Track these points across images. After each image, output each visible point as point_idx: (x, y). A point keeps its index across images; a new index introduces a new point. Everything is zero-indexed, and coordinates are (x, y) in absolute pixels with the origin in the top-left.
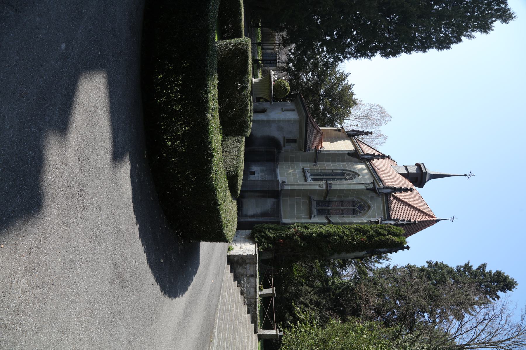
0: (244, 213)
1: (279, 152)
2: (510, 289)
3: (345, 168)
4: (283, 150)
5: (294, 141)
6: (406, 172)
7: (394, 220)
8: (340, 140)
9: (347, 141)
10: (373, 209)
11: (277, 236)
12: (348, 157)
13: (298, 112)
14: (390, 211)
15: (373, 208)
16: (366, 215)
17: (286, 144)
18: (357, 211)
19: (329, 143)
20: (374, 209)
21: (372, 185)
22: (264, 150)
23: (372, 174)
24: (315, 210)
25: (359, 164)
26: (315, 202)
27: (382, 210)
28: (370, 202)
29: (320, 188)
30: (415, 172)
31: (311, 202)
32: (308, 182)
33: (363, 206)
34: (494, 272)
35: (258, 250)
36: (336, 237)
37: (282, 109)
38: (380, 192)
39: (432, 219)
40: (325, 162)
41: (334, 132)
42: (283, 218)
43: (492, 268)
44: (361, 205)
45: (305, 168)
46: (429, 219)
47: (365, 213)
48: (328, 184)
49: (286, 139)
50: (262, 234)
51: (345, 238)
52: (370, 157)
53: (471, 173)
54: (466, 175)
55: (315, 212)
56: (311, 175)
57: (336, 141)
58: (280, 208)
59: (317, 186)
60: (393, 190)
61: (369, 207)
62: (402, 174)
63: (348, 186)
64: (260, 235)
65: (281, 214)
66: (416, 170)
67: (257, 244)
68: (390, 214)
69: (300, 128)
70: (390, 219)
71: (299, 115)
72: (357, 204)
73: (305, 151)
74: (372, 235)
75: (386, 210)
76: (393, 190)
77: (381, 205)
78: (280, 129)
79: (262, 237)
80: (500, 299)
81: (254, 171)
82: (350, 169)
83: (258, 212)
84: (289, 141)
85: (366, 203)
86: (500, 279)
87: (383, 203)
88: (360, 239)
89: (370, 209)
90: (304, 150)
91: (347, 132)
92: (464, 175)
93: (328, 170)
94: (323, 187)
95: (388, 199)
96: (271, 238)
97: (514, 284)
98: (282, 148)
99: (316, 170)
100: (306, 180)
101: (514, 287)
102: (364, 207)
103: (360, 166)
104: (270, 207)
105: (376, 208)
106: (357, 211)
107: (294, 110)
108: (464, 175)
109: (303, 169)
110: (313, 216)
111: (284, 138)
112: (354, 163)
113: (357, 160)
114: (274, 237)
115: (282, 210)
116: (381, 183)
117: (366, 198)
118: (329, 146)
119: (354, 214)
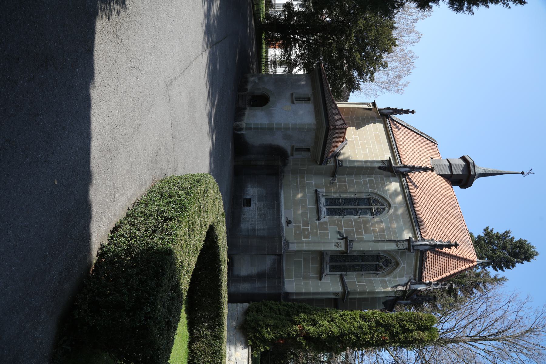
0: (236, 273)
1: (285, 165)
2: (528, 260)
3: (373, 190)
4: (291, 158)
5: (308, 150)
6: (449, 173)
7: (426, 284)
10: (402, 266)
12: (379, 170)
13: (316, 106)
15: (402, 265)
16: (392, 274)
17: (295, 153)
18: (381, 268)
21: (407, 243)
22: (263, 164)
23: (407, 204)
24: (328, 266)
27: (413, 268)
28: (399, 259)
29: (338, 249)
30: (461, 173)
31: (324, 257)
33: (390, 261)
34: (516, 240)
36: (351, 335)
38: (415, 249)
39: (471, 265)
40: (346, 176)
41: (362, 111)
43: (517, 236)
45: (319, 190)
46: (467, 266)
47: (392, 272)
48: (348, 241)
50: (257, 335)
51: (363, 336)
52: (408, 169)
53: (531, 171)
54: (523, 173)
55: (324, 212)
56: (327, 199)
59: (334, 244)
60: (432, 248)
61: (397, 264)
63: (375, 243)
64: (254, 336)
66: (462, 171)
68: (422, 275)
69: (317, 137)
70: (420, 282)
71: (317, 114)
72: (382, 258)
73: (321, 164)
74: (397, 332)
76: (432, 248)
77: (414, 262)
78: (287, 137)
80: (514, 268)
81: (249, 197)
83: (253, 272)
84: (298, 149)
85: (394, 258)
86: (522, 251)
87: (417, 260)
88: (381, 337)
89: (398, 267)
90: (319, 163)
91: (380, 110)
92: (521, 173)
93: (349, 192)
94: (341, 247)
95: (423, 256)
96: (268, 340)
97: (533, 254)
98: (289, 157)
100: (319, 219)
102: (390, 263)
103: (394, 186)
104: (269, 266)
105: (405, 265)
106: (381, 268)
108: (521, 173)
109: (316, 190)
111: (293, 147)
113: (390, 173)
115: (285, 268)
116: (417, 228)
119: (376, 271)
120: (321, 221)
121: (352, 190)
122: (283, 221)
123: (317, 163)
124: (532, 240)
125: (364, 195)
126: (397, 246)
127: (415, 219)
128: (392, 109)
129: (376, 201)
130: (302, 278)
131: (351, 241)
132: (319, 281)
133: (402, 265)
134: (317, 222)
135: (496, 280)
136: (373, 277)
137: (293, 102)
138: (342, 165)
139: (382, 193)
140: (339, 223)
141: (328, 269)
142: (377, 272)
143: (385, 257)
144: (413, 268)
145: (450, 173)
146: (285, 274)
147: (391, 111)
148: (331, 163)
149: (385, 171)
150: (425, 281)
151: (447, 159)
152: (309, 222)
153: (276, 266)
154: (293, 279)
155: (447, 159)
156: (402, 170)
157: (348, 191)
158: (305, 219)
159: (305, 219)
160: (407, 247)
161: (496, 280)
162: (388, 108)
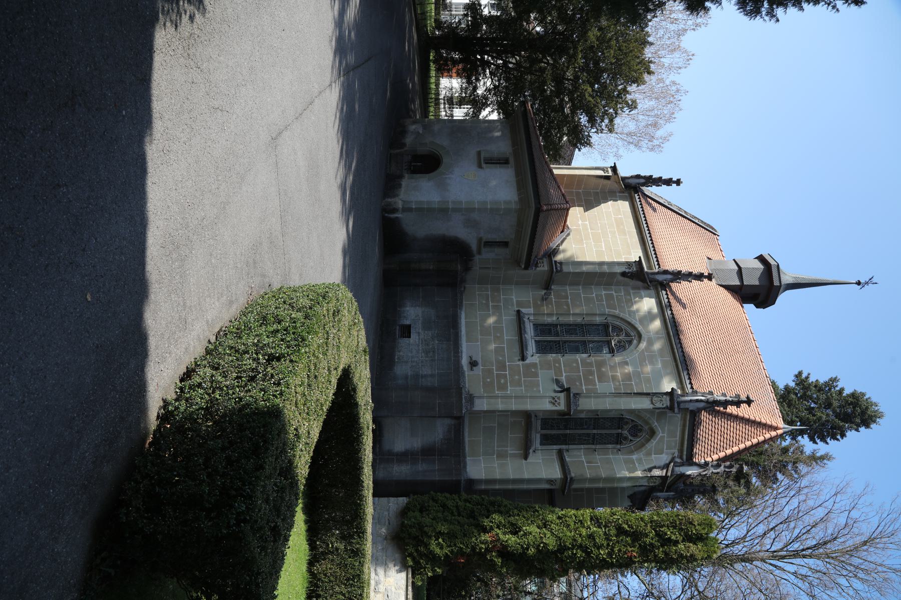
0: (386, 446)
1: (467, 269)
2: (867, 426)
4: (477, 258)
5: (505, 244)
6: (737, 283)
7: (699, 465)
8: (606, 200)
9: (620, 202)
11: (452, 552)
13: (519, 173)
14: (695, 445)
15: (661, 435)
17: (483, 250)
18: (626, 438)
19: (582, 209)
20: (663, 437)
21: (668, 398)
24: (538, 436)
25: (643, 292)
26: (539, 422)
28: (656, 424)
29: (554, 408)
30: (757, 283)
31: (531, 422)
32: (526, 362)
33: (640, 427)
34: (847, 392)
35: (413, 582)
36: (577, 550)
37: (479, 153)
39: (773, 434)
40: (568, 288)
42: (467, 454)
43: (848, 386)
44: (635, 425)
45: (523, 310)
46: (768, 436)
47: (643, 445)
49: (484, 240)
50: (422, 549)
51: (595, 551)
52: (669, 277)
54: (859, 283)
55: (531, 347)
56: (536, 326)
57: (598, 203)
58: (463, 435)
59: (547, 400)
60: (709, 405)
61: (652, 433)
62: (727, 287)
63: (615, 398)
64: (417, 551)
65: (465, 447)
66: (760, 279)
67: (410, 570)
71: (520, 186)
72: (627, 423)
73: (526, 268)
74: (651, 544)
75: (687, 433)
79: (421, 555)
81: (407, 322)
82: (622, 315)
84: (489, 244)
85: (647, 423)
87: (684, 426)
88: (625, 553)
90: (523, 266)
91: (624, 179)
92: (856, 283)
94: (559, 404)
95: (695, 420)
97: (875, 416)
99: (547, 314)
100: (523, 358)
101: (875, 422)
102: (641, 430)
103: (647, 304)
104: (441, 436)
106: (626, 438)
107: (502, 162)
108: (856, 283)
109: (518, 312)
110: (531, 451)
111: (480, 240)
112: (631, 291)
113: (640, 283)
114: (446, 556)
115: (467, 439)
116: (685, 373)
117: (648, 416)
118: (580, 222)
120: (527, 361)
121: (577, 311)
122: (465, 361)
123: (521, 267)
124: (874, 393)
125: (598, 320)
126: (652, 403)
127: (682, 359)
128: (644, 177)
129: (618, 330)
130: (495, 456)
131: (576, 395)
132: (524, 461)
133: (660, 434)
134: (521, 363)
135: (815, 459)
136: (613, 453)
137: (480, 166)
138: (561, 270)
139: (628, 316)
140: (557, 365)
141: (538, 441)
142: (618, 446)
143: (632, 421)
144: (678, 438)
145: (739, 284)
146: (467, 449)
147: (642, 181)
148: (543, 266)
149: (632, 279)
150: (697, 461)
151: (734, 260)
152: (507, 364)
153: (453, 436)
154: (481, 458)
155: (734, 260)
156: (661, 278)
157: (571, 312)
158: (501, 358)
159: (501, 358)
160: (668, 404)
161: (815, 459)
162: (638, 177)
